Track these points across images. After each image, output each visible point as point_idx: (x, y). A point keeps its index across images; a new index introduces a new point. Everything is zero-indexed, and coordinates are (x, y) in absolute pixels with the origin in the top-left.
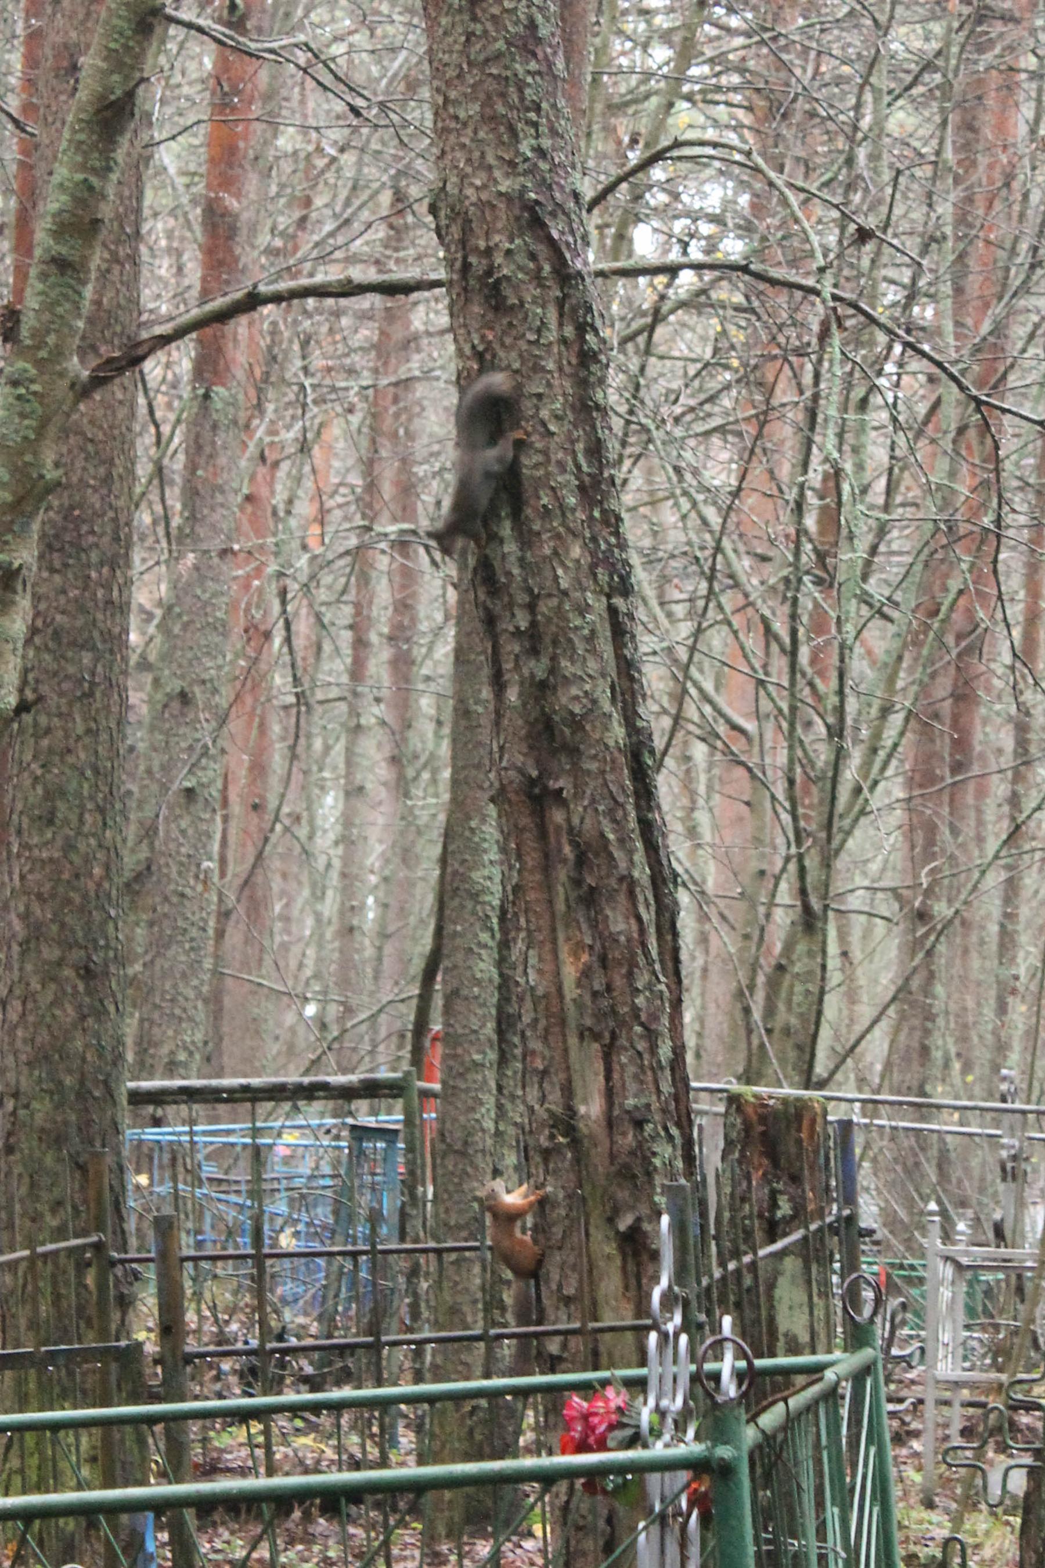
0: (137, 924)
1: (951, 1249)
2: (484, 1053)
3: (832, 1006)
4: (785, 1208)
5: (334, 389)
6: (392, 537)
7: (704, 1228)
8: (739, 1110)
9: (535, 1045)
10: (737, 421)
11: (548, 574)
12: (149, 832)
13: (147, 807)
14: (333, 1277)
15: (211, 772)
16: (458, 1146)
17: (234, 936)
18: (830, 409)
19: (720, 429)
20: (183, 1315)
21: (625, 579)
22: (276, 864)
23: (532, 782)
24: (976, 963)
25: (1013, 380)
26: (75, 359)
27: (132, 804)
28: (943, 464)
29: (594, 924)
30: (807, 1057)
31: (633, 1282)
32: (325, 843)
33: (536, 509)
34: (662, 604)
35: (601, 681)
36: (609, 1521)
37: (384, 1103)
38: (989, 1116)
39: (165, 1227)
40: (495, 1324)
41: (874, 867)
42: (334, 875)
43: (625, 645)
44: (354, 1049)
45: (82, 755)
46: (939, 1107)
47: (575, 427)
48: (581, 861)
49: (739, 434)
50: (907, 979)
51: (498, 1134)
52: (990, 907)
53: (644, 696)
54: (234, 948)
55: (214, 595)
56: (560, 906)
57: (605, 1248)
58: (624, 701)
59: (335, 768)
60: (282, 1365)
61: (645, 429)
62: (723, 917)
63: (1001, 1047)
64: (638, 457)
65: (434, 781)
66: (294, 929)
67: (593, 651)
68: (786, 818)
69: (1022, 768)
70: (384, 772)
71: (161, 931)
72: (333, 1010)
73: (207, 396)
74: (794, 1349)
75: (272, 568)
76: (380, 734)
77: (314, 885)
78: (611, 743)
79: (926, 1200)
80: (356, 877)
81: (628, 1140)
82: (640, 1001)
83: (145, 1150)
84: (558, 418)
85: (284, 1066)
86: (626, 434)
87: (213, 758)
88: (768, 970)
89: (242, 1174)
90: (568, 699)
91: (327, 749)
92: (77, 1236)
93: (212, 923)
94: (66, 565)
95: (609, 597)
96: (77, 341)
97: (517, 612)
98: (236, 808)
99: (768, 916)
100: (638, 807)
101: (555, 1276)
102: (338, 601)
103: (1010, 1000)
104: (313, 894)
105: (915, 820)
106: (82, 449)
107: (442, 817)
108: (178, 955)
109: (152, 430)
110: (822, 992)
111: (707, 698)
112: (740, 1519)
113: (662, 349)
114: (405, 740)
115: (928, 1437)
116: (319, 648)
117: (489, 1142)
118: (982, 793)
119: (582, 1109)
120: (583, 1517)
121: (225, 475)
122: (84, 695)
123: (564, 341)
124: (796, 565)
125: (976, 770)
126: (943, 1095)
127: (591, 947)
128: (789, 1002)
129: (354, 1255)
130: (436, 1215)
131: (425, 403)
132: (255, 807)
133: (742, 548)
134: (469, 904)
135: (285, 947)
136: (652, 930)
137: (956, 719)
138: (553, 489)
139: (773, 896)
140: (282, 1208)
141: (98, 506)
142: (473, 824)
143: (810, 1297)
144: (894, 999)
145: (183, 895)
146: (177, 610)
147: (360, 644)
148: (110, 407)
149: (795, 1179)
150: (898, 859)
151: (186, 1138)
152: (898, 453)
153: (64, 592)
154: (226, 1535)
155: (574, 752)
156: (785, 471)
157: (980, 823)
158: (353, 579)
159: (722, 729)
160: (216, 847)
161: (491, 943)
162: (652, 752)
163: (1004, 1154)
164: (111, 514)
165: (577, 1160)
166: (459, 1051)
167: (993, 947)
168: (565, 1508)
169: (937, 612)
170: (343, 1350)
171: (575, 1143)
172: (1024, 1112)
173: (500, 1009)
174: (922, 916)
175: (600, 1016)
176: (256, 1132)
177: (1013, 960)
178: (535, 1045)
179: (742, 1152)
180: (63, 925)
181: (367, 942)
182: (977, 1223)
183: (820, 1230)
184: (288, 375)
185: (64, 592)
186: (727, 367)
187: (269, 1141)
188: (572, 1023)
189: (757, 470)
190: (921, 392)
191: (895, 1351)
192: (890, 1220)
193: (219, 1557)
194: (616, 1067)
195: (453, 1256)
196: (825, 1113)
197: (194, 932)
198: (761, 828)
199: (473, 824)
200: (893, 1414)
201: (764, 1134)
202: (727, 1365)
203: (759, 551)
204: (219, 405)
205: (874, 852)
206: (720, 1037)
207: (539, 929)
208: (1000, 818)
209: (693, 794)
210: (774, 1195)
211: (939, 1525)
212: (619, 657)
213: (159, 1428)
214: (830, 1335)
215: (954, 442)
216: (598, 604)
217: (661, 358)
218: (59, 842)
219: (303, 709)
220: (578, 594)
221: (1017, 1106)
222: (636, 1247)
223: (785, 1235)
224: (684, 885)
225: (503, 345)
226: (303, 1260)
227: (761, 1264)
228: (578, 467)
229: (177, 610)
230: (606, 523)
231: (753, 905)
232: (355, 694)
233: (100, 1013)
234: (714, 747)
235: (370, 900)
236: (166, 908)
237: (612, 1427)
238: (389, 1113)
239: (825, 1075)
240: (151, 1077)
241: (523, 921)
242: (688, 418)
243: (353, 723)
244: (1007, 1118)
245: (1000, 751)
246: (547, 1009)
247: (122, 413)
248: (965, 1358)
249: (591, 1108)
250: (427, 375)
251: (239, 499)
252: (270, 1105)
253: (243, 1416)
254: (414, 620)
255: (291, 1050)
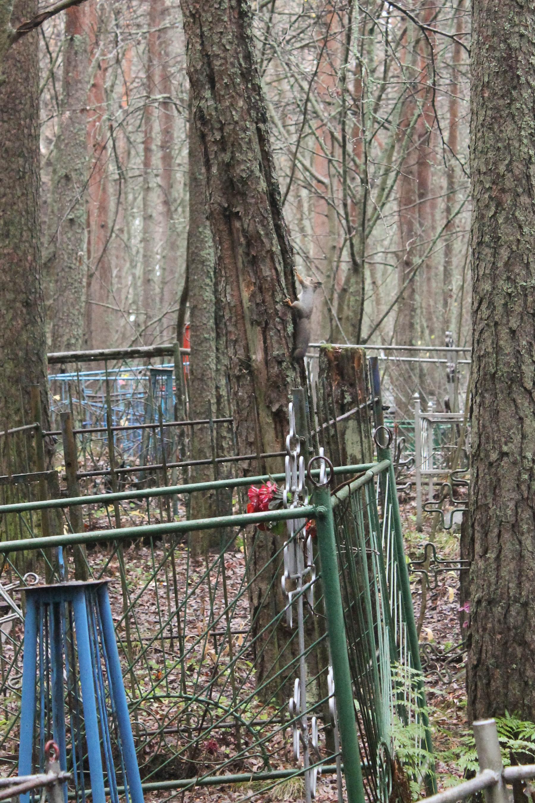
0: (50, 281)
1: (426, 414)
2: (209, 333)
3: (368, 306)
4: (348, 398)
5: (130, 34)
6: (161, 100)
7: (311, 408)
8: (326, 355)
9: (231, 328)
10: (314, 42)
11: (228, 114)
12: (53, 239)
13: (52, 228)
14: (145, 438)
15: (81, 211)
16: (199, 377)
17: (95, 286)
18: (355, 35)
19: (307, 45)
20: (77, 458)
21: (263, 115)
22: (113, 252)
23: (225, 209)
24: (434, 285)
25: (440, 17)
26: (10, 24)
27: (44, 227)
28: (409, 57)
29: (256, 273)
30: (357, 330)
31: (280, 434)
32: (135, 242)
33: (221, 85)
34: (284, 126)
35: (254, 162)
36: (274, 543)
37: (166, 358)
38: (442, 353)
39: (66, 418)
40: (218, 456)
41: (386, 243)
42: (140, 256)
43: (265, 145)
44: (152, 335)
45: (21, 205)
46: (420, 350)
47: (238, 46)
48: (249, 244)
49: (315, 47)
50: (402, 293)
51: (217, 370)
52: (439, 258)
53: (274, 168)
54: (95, 291)
55: (79, 130)
56: (240, 265)
57: (267, 420)
58: (265, 171)
59: (139, 208)
60: (125, 479)
61: (272, 47)
62: (317, 268)
63: (447, 322)
64: (271, 59)
65: (184, 212)
66: (123, 281)
67: (250, 149)
68: (344, 222)
69: (451, 195)
70: (161, 208)
71: (61, 284)
72: (142, 318)
73: (72, 39)
74: (355, 462)
75: (105, 117)
76: (158, 191)
77: (132, 261)
78: (260, 190)
79: (413, 392)
80: (150, 256)
81: (275, 370)
82: (278, 307)
83: (58, 384)
84: (231, 43)
85: (122, 344)
86: (264, 50)
87: (82, 205)
88: (339, 291)
89: (102, 394)
90: (240, 171)
91: (135, 199)
92: (27, 424)
93: (85, 280)
94: (9, 119)
95: (257, 123)
96: (10, 16)
97: (215, 131)
98: (93, 226)
99: (338, 267)
100: (274, 219)
101: (244, 434)
102: (137, 131)
103: (449, 300)
104: (131, 264)
105: (403, 220)
106: (15, 66)
107: (188, 228)
108: (70, 295)
109: (49, 56)
110: (363, 300)
111: (306, 169)
112: (330, 538)
113: (280, 10)
114: (170, 193)
115: (419, 499)
116: (129, 153)
117: (213, 374)
118: (433, 207)
119: (254, 357)
120: (261, 542)
121: (82, 75)
122: (20, 178)
123: (231, 7)
124: (343, 106)
125: (430, 196)
126: (421, 345)
127: (255, 283)
128: (348, 306)
129: (154, 427)
130: (190, 408)
131: (173, 39)
132: (103, 226)
133: (319, 99)
134: (200, 266)
135: (119, 290)
136: (282, 274)
137: (420, 173)
138: (229, 75)
139: (340, 257)
140: (122, 408)
141: (23, 91)
142: (200, 230)
143: (361, 438)
144: (396, 301)
145: (70, 268)
146: (62, 137)
147: (147, 150)
148: (26, 46)
149: (352, 385)
150: (396, 238)
151: (76, 378)
152: (388, 54)
153: (9, 131)
154: (101, 557)
155: (244, 195)
156: (338, 63)
157: (434, 220)
158: (143, 121)
159: (314, 183)
160: (85, 246)
161: (211, 284)
162: (279, 193)
163: (448, 370)
164: (29, 95)
165: (252, 380)
166: (198, 333)
167: (442, 277)
168: (253, 538)
169: (409, 125)
170: (152, 470)
171: (251, 373)
172: (457, 351)
173: (216, 313)
174: (408, 264)
175: (260, 314)
176: (108, 374)
177: (450, 282)
178: (231, 328)
179: (328, 373)
180: (15, 283)
181: (157, 287)
182: (438, 403)
183: (364, 407)
184: (109, 29)
185: (9, 131)
186: (309, 17)
187: (114, 378)
188: (247, 318)
189: (324, 64)
190: (399, 25)
191: (401, 461)
192: (398, 402)
193: (98, 567)
194: (268, 337)
195: (200, 426)
196: (365, 355)
197: (76, 285)
198: (334, 227)
199: (200, 230)
200: (400, 490)
201: (337, 365)
202: (322, 470)
203: (327, 100)
204: (78, 43)
205: (385, 235)
206: (318, 323)
207: (231, 276)
208: (442, 219)
209: (302, 214)
210: (343, 392)
211: (425, 539)
212: (263, 151)
213: (66, 510)
214: (371, 455)
215: (414, 47)
216: (252, 127)
217: (279, 14)
218: (12, 246)
219: (123, 181)
220: (242, 123)
221: (454, 348)
222: (280, 418)
223: (349, 410)
224: (298, 254)
225: (204, 10)
226: (131, 431)
227: (338, 424)
228: (240, 65)
229: (62, 137)
230: (254, 90)
231: (330, 262)
232: (146, 173)
233: (33, 323)
234: (310, 191)
235: (157, 267)
236: (63, 273)
237: (270, 500)
238: (169, 363)
239: (366, 338)
240: (59, 350)
241: (223, 272)
242: (293, 40)
243: (146, 186)
244: (449, 354)
245: (441, 188)
246: (236, 312)
247: (32, 48)
248: (434, 464)
249: (258, 357)
250: (173, 26)
251: (89, 87)
252: (115, 362)
253: (106, 502)
254: (172, 138)
255: (124, 337)
